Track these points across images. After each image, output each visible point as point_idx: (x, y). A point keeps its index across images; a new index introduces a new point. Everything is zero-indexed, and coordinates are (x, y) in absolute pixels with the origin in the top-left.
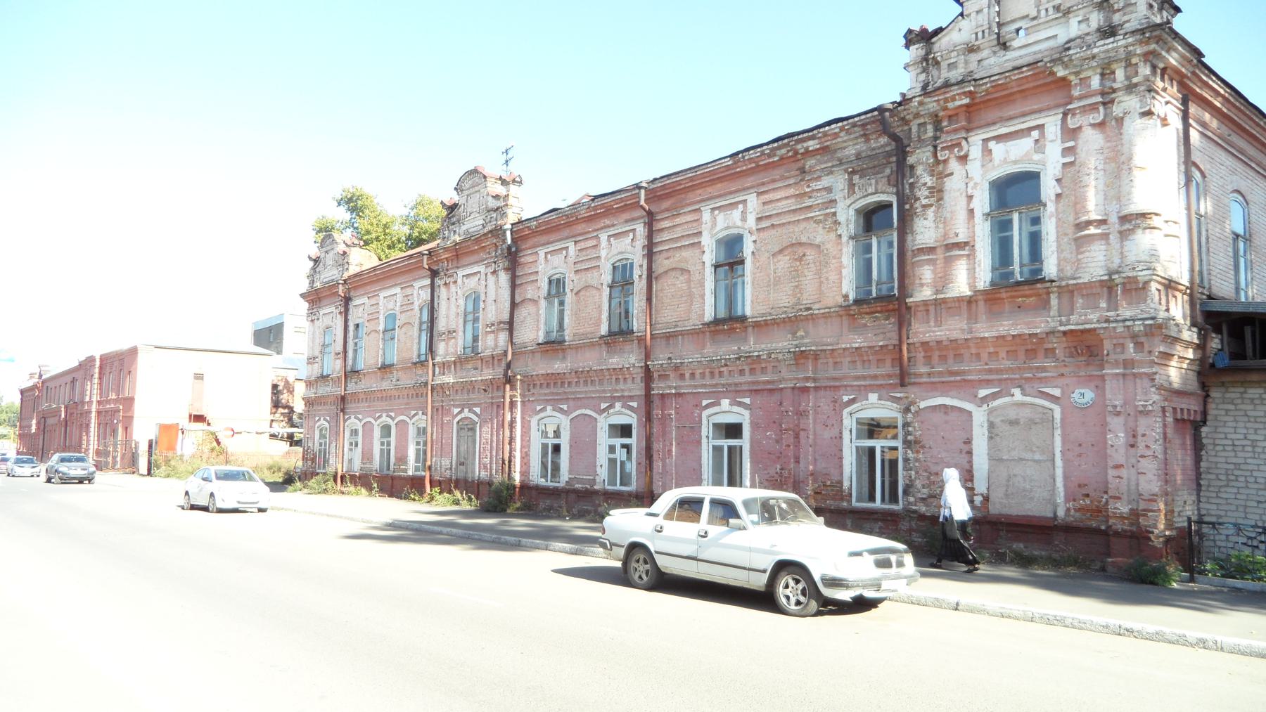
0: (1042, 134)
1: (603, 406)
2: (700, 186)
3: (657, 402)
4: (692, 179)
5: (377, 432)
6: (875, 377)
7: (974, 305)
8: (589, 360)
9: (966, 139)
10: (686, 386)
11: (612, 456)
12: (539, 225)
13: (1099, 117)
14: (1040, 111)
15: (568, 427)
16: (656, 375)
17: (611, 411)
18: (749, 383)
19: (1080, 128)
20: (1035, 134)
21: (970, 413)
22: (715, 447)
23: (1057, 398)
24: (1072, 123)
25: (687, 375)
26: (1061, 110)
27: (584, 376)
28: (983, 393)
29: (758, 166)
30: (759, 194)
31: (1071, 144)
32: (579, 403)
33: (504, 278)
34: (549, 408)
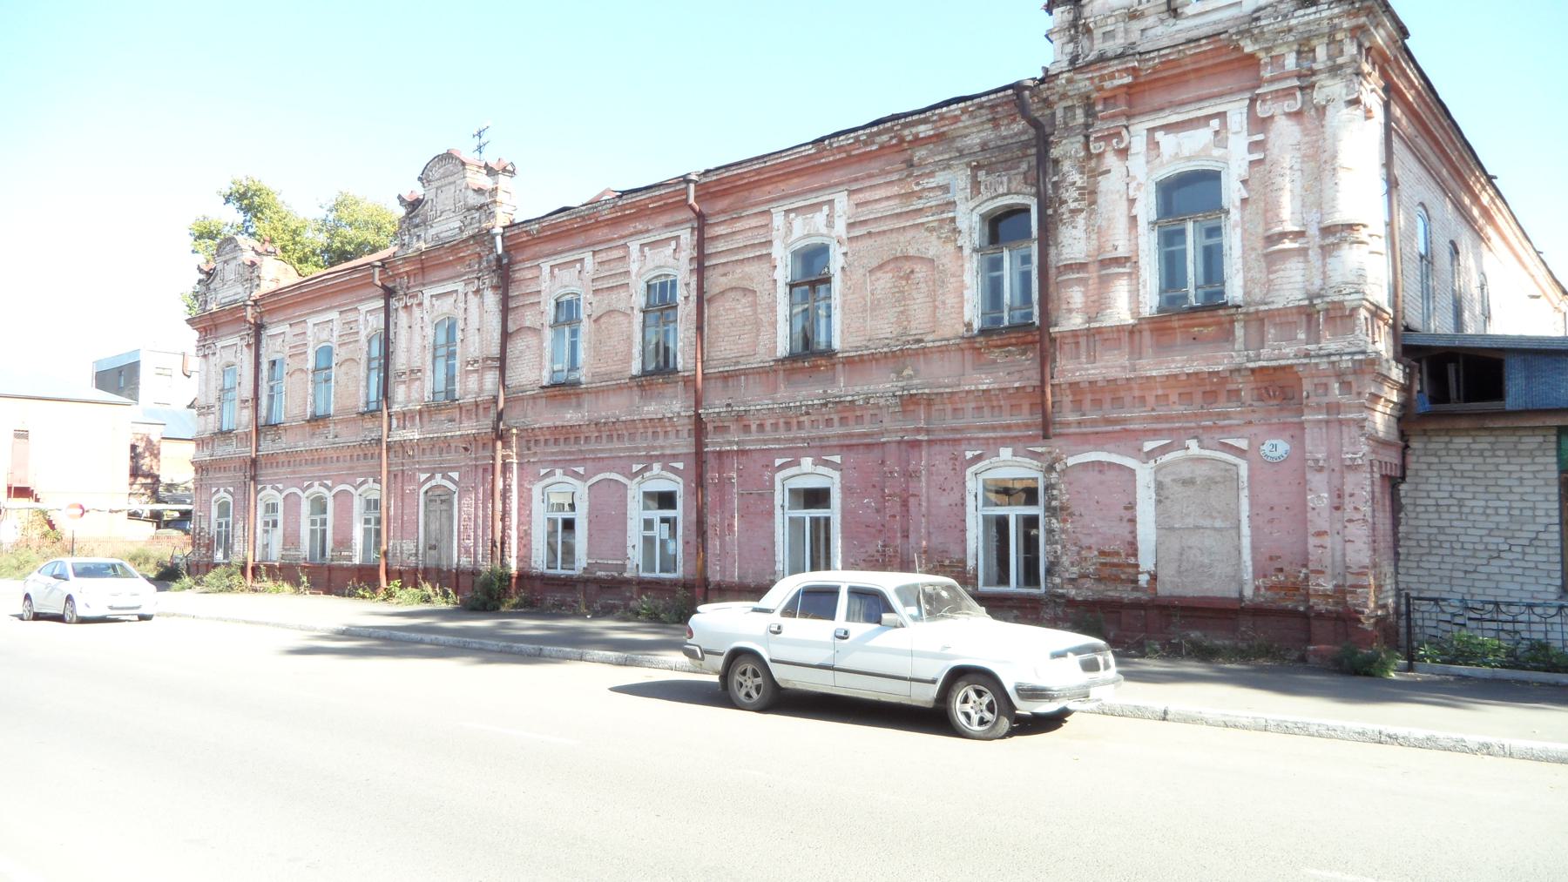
0: (1224, 124)
1: (636, 468)
3: (712, 462)
4: (758, 172)
8: (616, 408)
11: (648, 533)
15: (586, 497)
16: (710, 427)
17: (647, 474)
19: (1272, 117)
20: (1215, 123)
21: (1132, 472)
24: (1262, 110)
25: (754, 427)
26: (1248, 95)
27: (609, 429)
28: (1149, 446)
29: (850, 156)
30: (851, 192)
31: (1260, 137)
32: (601, 464)
33: (491, 299)
34: (559, 472)
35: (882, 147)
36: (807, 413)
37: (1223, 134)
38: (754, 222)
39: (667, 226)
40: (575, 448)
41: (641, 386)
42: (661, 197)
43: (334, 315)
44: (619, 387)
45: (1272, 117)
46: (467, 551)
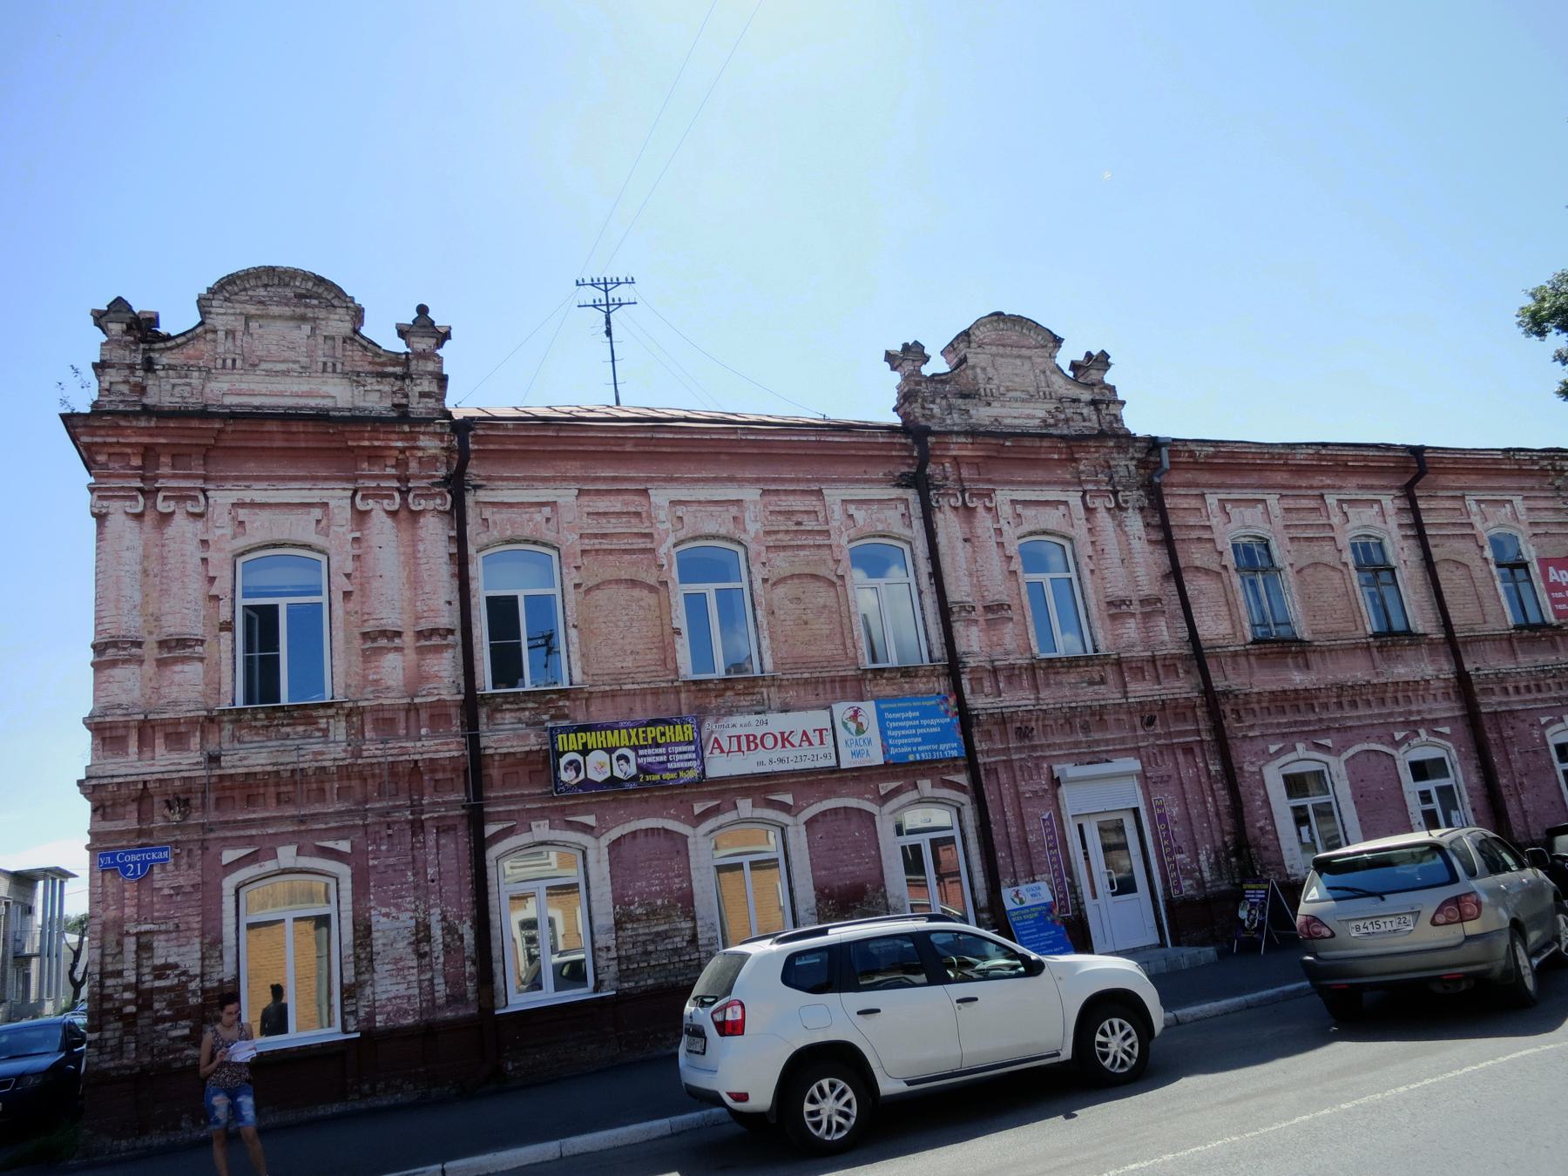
0: (326, 514)
1: (1398, 736)
2: (1455, 471)
3: (1487, 724)
4: (1455, 461)
5: (130, 944)
6: (1279, 725)
7: (412, 714)
8: (1356, 671)
9: (204, 491)
10: (1516, 702)
11: (1428, 807)
12: (1215, 455)
13: (396, 503)
14: (1510, 489)
15: (1344, 772)
16: (495, 773)
17: (1415, 742)
18: (339, 813)
19: (173, 513)
20: (547, 511)
21: (871, 816)
22: (1295, 809)
23: (592, 828)
24: (360, 505)
25: (1511, 689)
26: (351, 486)
27: (1347, 694)
28: (885, 787)
29: (1285, 464)
30: (1526, 498)
31: (358, 534)
32: (1349, 735)
33: (435, 533)
34: (1300, 746)
35: (1541, 469)
36: (1554, 676)
37: (324, 523)
38: (1448, 504)
39: (1361, 487)
40: (1312, 717)
41: (1380, 648)
42: (1365, 458)
43: (751, 494)
44: (1356, 647)
45: (173, 513)
46: (1189, 874)
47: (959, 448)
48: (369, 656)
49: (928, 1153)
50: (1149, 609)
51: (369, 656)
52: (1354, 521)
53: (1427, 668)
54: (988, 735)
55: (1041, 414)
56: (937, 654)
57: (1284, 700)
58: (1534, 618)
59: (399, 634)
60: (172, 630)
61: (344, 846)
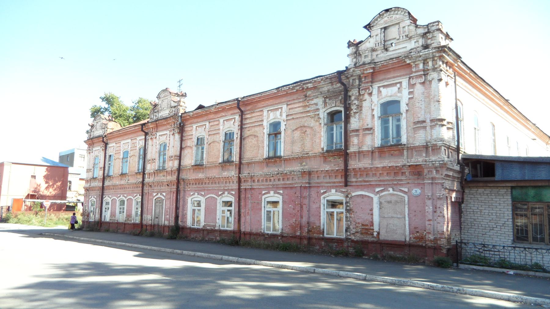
1: (220, 193)
2: (263, 100)
6: (334, 183)
8: (214, 173)
9: (371, 86)
10: (256, 185)
11: (223, 215)
16: (243, 180)
19: (415, 84)
21: (372, 198)
25: (256, 181)
27: (212, 180)
33: (177, 136)
35: (297, 91)
45: (415, 84)
47: (151, 126)
48: (415, 130)
49: (104, 247)
50: (433, 124)
51: (415, 130)
52: (226, 127)
53: (232, 173)
54: (355, 175)
55: (168, 112)
56: (140, 168)
57: (199, 182)
58: (278, 154)
59: (424, 122)
60: (434, 116)
61: (281, 192)
